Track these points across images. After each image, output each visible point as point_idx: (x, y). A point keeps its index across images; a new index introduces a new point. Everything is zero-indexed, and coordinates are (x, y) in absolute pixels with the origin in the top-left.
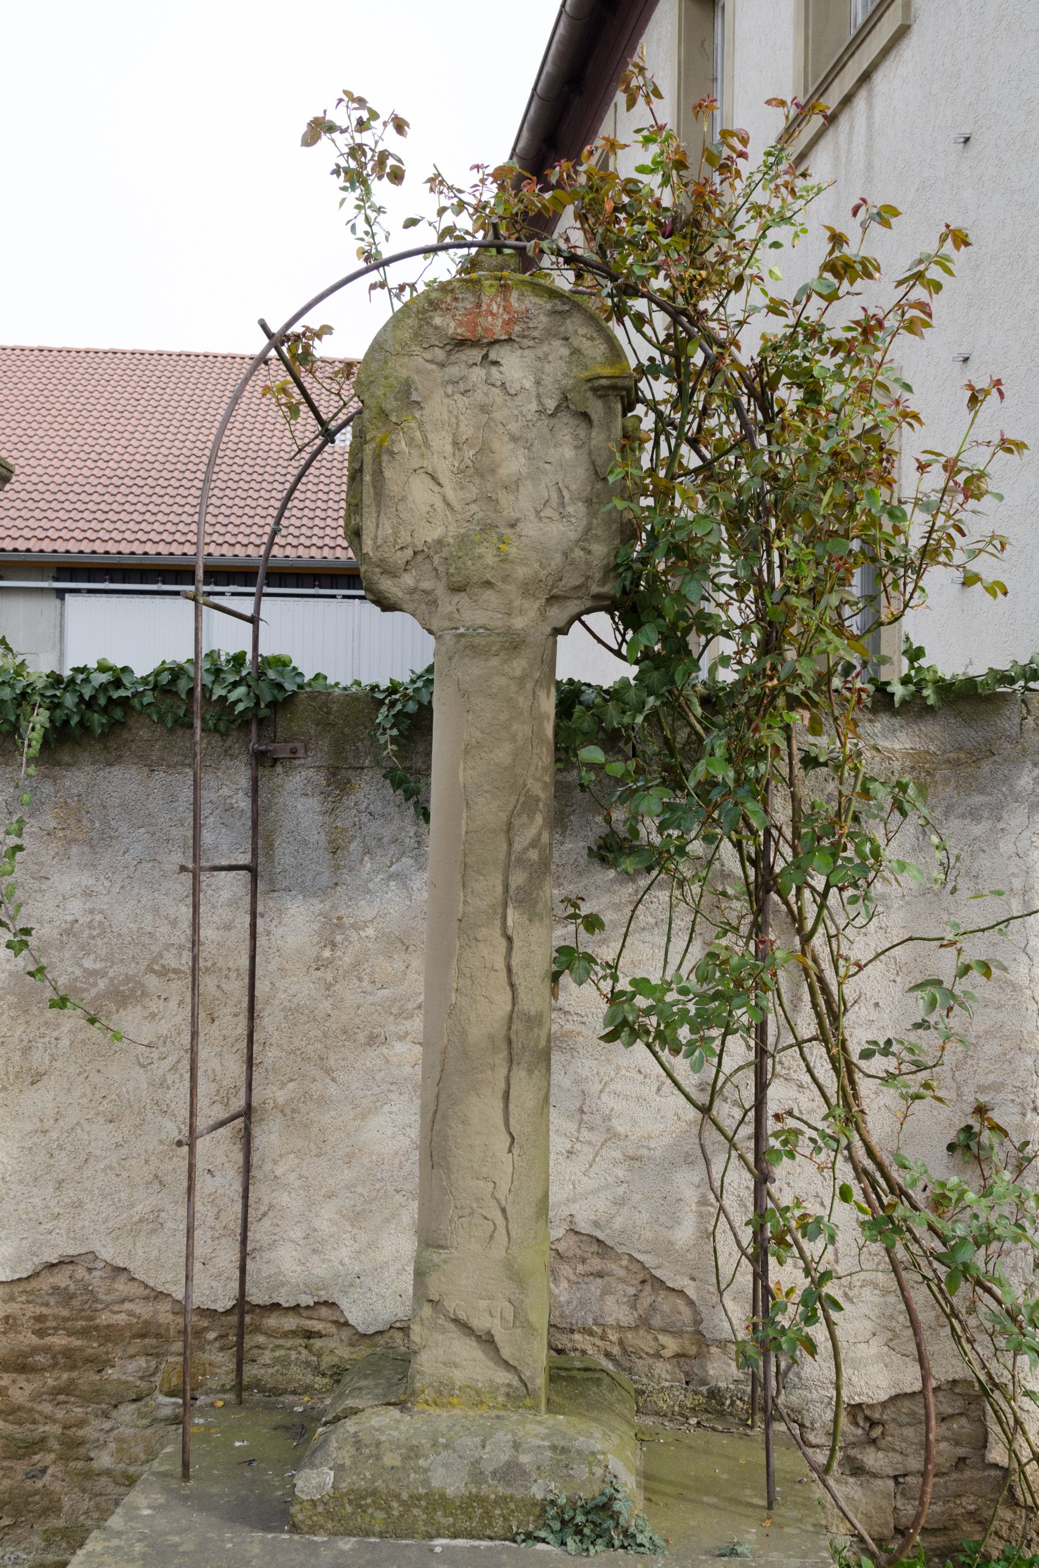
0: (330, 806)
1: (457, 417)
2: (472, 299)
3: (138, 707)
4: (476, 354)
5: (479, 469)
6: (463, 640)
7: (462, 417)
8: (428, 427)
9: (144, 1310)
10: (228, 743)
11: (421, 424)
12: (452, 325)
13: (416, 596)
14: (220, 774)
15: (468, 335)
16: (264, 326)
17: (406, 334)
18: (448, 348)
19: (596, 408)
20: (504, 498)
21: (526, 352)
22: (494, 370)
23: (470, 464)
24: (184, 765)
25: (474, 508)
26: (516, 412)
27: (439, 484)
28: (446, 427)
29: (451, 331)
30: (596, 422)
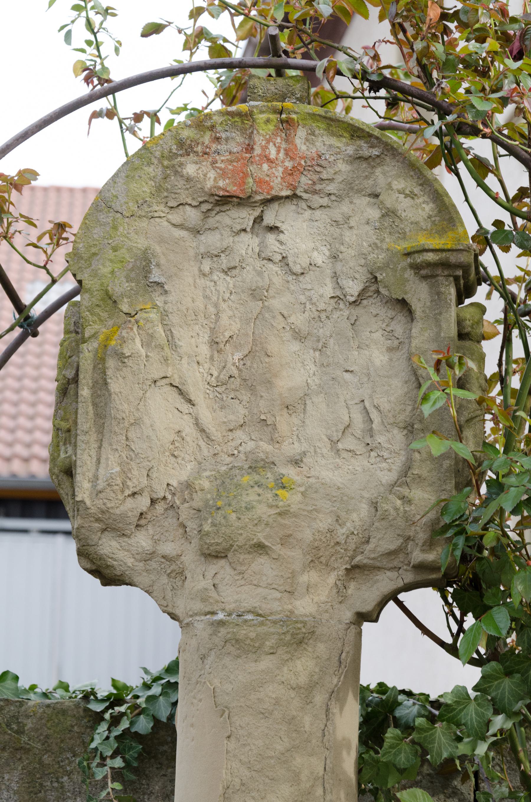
1: (216, 305)
2: (240, 139)
4: (245, 216)
5: (246, 378)
6: (223, 631)
7: (223, 306)
8: (175, 319)
12: (212, 175)
13: (154, 564)
15: (233, 189)
18: (205, 207)
19: (419, 294)
20: (284, 423)
21: (318, 213)
22: (271, 238)
25: (240, 435)
26: (302, 298)
27: (190, 401)
28: (201, 319)
29: (209, 184)
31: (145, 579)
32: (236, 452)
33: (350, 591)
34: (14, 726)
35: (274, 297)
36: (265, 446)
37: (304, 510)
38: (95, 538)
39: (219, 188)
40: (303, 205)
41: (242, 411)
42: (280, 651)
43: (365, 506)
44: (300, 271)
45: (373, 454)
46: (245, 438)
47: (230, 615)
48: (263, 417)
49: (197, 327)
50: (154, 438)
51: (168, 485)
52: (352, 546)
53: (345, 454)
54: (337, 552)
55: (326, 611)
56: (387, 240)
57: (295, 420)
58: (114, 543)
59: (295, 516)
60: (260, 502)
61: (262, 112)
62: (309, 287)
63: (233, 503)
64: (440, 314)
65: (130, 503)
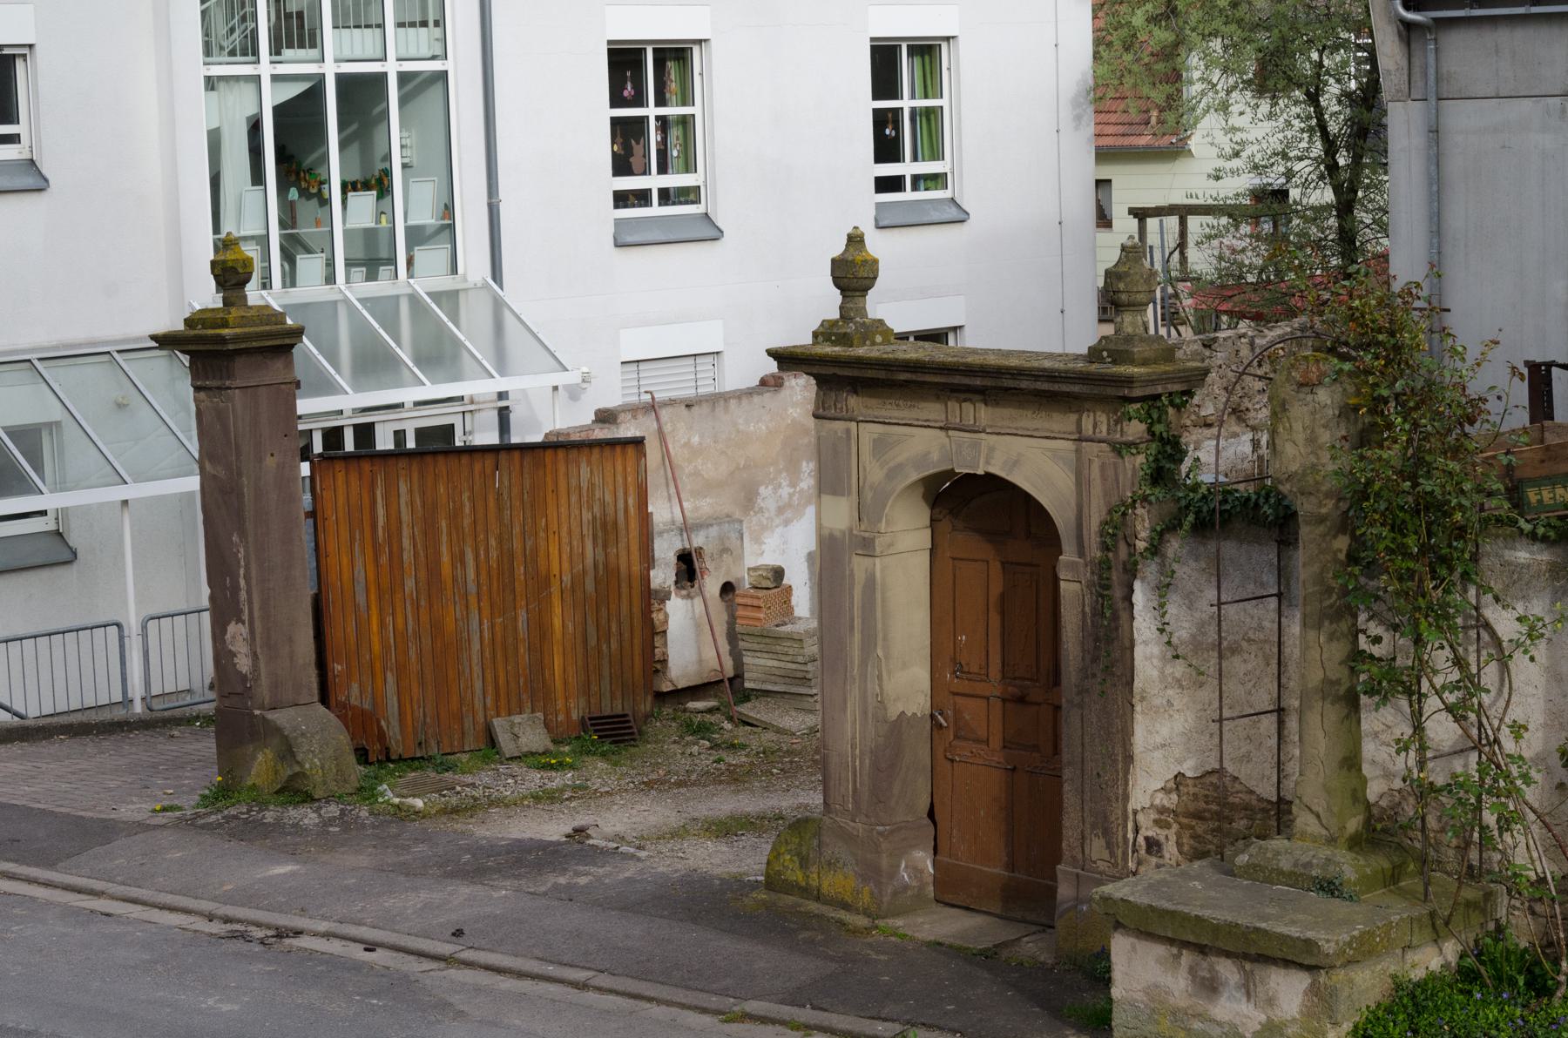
4: (1307, 389)
5: (1312, 440)
9: (1246, 797)
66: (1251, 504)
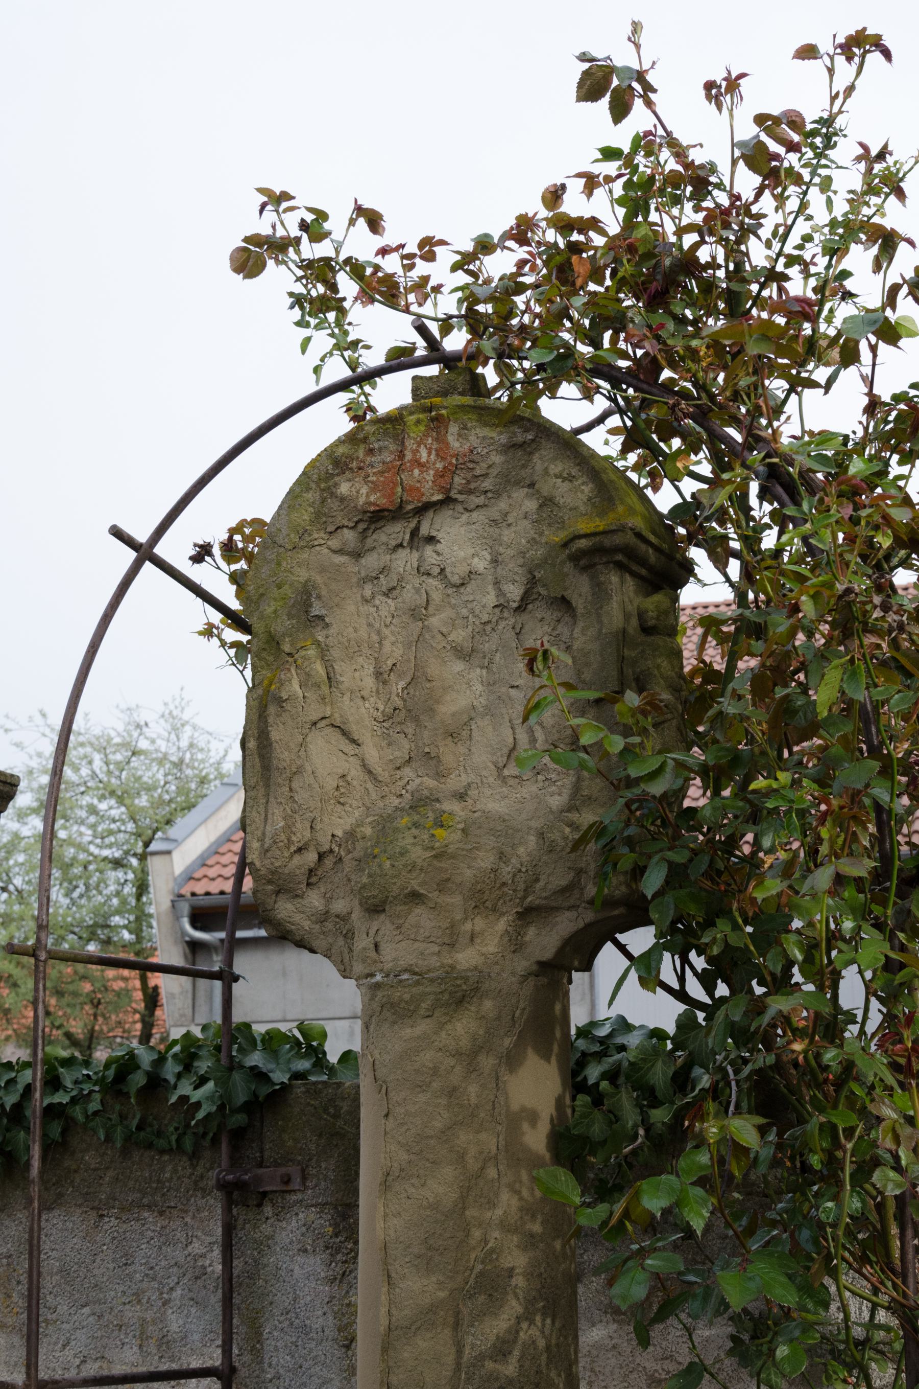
0: (339, 1269)
1: (379, 632)
2: (393, 447)
3: (80, 1118)
4: (398, 531)
5: (411, 711)
6: (380, 994)
7: (386, 631)
8: (336, 653)
10: (200, 1170)
11: (323, 651)
12: (364, 491)
13: (329, 925)
14: (188, 1219)
15: (384, 502)
16: (117, 533)
17: (305, 516)
18: (361, 526)
19: (579, 589)
20: (449, 753)
21: (475, 514)
22: (429, 550)
23: (399, 703)
24: (142, 1206)
25: (408, 772)
26: (465, 612)
27: (354, 741)
28: (365, 650)
29: (362, 500)
30: (580, 610)
31: (320, 943)
32: (404, 792)
33: (527, 938)
34: (332, 1110)
35: (434, 615)
36: (430, 783)
37: (463, 850)
38: (270, 901)
39: (370, 504)
40: (459, 508)
41: (406, 745)
42: (437, 1014)
43: (532, 838)
44: (459, 582)
45: (540, 777)
46: (412, 775)
47: (387, 976)
48: (427, 750)
49: (360, 660)
50: (316, 786)
51: (333, 836)
52: (522, 886)
53: (511, 782)
54: (505, 894)
55: (497, 963)
56: (546, 533)
57: (461, 749)
58: (289, 906)
59: (453, 857)
60: (414, 844)
61: (411, 413)
62: (471, 598)
63: (389, 848)
64: (601, 608)
65: (297, 860)
66: (138, 1080)
